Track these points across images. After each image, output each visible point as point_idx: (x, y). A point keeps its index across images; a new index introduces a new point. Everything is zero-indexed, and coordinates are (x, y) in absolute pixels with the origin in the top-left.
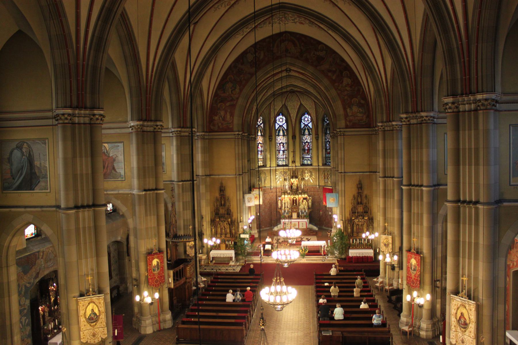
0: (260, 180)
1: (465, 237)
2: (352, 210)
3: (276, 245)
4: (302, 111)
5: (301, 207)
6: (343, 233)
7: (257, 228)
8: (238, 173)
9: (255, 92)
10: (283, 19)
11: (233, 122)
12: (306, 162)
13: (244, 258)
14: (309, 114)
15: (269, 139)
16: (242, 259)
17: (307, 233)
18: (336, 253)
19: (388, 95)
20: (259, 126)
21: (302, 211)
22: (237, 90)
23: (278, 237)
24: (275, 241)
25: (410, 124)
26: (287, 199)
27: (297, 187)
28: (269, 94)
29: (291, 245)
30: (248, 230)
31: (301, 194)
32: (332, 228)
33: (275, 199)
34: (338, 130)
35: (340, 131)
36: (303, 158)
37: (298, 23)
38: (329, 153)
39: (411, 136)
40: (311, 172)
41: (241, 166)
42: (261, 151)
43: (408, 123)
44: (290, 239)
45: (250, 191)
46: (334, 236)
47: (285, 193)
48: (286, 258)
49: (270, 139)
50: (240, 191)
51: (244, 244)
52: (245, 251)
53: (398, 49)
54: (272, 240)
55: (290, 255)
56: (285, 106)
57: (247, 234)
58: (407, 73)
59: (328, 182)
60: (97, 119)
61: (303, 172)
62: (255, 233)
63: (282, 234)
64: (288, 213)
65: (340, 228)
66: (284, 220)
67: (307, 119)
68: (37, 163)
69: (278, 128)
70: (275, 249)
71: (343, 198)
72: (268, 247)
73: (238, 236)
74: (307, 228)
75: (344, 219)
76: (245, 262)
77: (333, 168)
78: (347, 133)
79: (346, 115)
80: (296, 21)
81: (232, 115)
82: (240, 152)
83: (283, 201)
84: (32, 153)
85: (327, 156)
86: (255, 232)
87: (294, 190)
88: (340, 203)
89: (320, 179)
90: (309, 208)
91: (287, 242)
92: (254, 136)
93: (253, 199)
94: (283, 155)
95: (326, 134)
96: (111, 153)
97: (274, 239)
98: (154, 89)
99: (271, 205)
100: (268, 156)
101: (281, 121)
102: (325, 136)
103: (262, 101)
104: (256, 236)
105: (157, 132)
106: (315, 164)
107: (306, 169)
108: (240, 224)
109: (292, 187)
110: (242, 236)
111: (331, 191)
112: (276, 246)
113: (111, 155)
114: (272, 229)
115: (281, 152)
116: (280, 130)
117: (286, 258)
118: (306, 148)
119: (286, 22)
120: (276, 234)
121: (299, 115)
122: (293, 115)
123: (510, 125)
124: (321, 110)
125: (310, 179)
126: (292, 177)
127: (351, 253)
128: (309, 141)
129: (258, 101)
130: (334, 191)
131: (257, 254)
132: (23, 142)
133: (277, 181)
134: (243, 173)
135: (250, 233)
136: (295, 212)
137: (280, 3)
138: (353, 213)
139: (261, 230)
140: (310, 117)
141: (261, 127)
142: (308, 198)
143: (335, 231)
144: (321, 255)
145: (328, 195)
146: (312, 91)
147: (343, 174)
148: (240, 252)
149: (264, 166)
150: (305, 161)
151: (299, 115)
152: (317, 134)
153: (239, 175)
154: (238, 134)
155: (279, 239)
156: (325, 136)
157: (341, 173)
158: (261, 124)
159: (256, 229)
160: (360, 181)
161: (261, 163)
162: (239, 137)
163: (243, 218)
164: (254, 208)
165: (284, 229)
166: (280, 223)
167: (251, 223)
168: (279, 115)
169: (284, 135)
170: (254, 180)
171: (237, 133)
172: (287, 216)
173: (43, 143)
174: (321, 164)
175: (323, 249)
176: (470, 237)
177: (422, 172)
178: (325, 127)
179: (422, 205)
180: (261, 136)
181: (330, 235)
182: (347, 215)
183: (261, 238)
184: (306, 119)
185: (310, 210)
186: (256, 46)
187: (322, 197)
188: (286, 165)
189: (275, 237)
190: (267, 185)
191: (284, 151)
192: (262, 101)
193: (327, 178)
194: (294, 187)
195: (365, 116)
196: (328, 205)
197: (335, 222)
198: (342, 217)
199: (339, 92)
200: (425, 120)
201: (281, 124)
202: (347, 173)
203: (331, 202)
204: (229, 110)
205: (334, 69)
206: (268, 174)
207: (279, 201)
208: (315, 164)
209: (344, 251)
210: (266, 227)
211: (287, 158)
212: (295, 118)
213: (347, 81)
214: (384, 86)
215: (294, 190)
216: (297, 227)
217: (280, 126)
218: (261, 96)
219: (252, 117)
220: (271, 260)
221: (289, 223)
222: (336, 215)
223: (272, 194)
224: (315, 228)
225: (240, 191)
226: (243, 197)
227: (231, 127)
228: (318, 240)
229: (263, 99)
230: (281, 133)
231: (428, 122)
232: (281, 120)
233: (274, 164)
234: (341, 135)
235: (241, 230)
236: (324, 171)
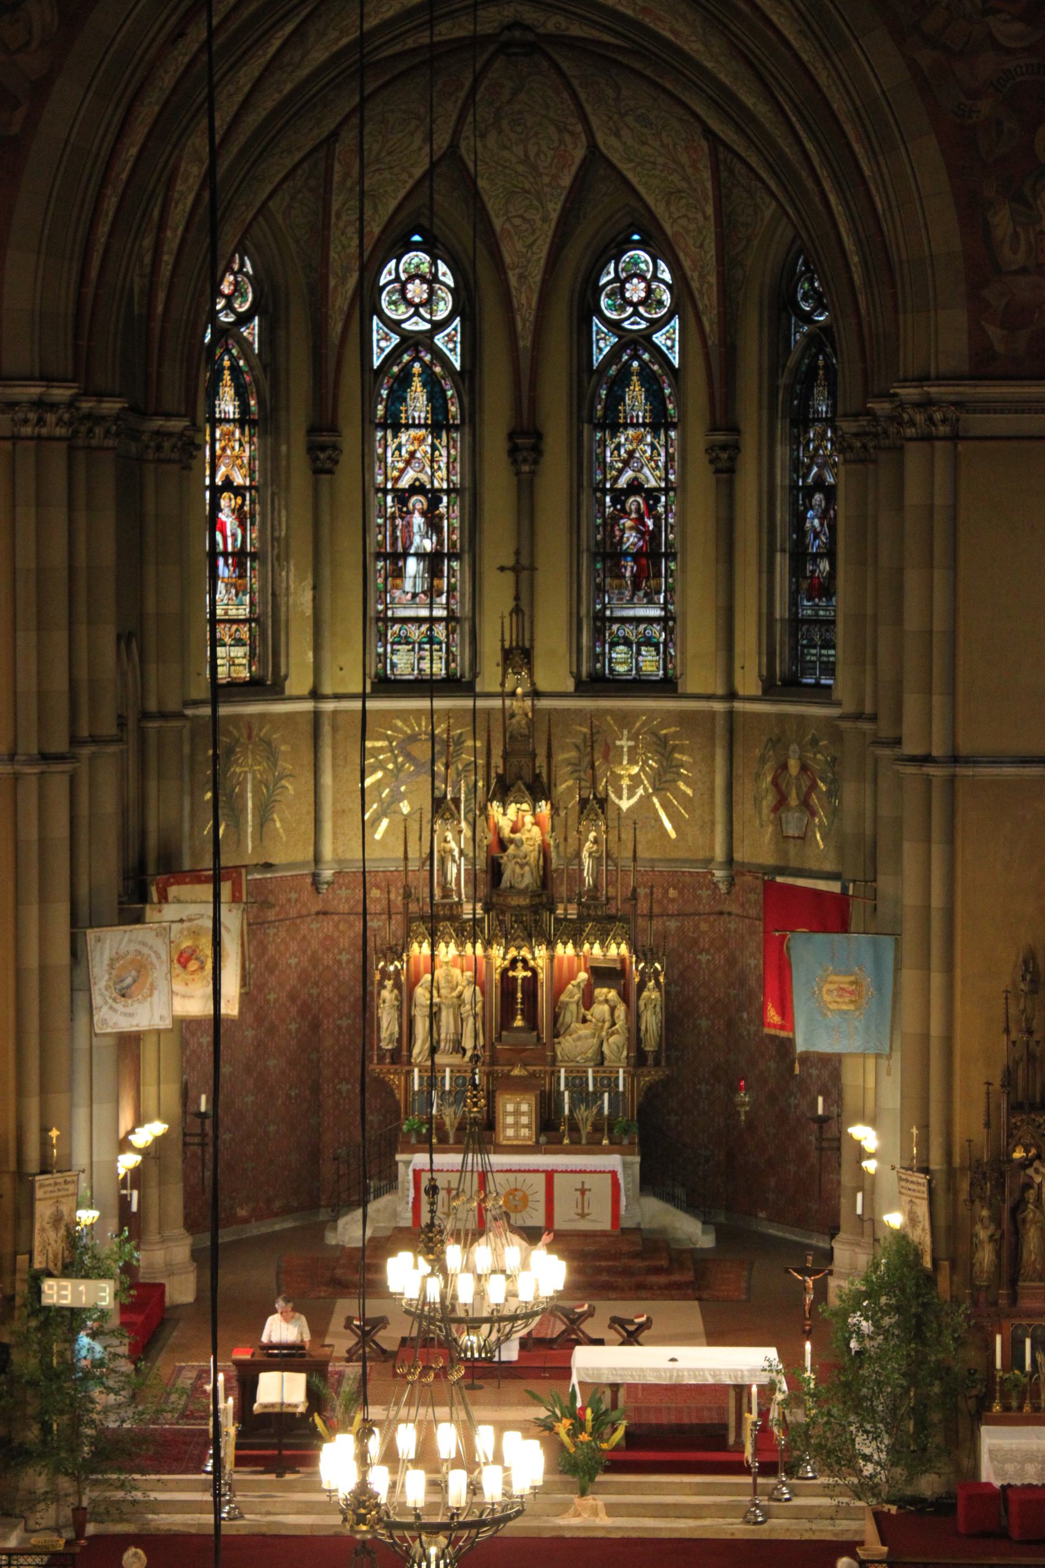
0: (223, 804)
2: (1009, 1078)
3: (353, 1370)
4: (603, 221)
5: (576, 1043)
6: (930, 1279)
7: (191, 1225)
8: (30, 746)
9: (198, 34)
12: (619, 661)
13: (65, 1483)
14: (660, 246)
15: (313, 449)
16: (54, 1496)
17: (619, 1274)
18: (871, 1448)
20: (222, 333)
21: (577, 1084)
23: (374, 1308)
24: (340, 1342)
26: (451, 968)
27: (546, 877)
28: (319, 56)
29: (485, 1372)
30: (107, 1244)
31: (575, 934)
32: (833, 1231)
33: (349, 973)
34: (909, 393)
35: (925, 404)
36: (601, 622)
38: (825, 589)
40: (663, 748)
41: (60, 683)
42: (240, 557)
44: (473, 1324)
45: (134, 899)
46: (855, 1302)
47: (437, 920)
48: (438, 1486)
49: (323, 457)
50: (44, 899)
51: (71, 1367)
52: (76, 1423)
54: (318, 1330)
55: (467, 1461)
56: (451, 168)
57: (102, 1274)
59: (803, 838)
61: (596, 749)
62: (170, 1270)
63: (405, 1275)
64: (457, 1096)
65: (900, 1237)
66: (420, 1160)
67: (639, 287)
70: (338, 1404)
71: (937, 979)
72: (280, 1390)
73: (22, 1289)
74: (621, 1232)
75: (936, 1163)
76: (79, 1528)
77: (858, 717)
78: (978, 423)
82: (58, 557)
83: (421, 993)
85: (806, 610)
86: (172, 1262)
87: (518, 903)
88: (910, 1021)
89: (744, 809)
90: (639, 1058)
91: (449, 1345)
92: (177, 425)
93: (159, 974)
94: (432, 592)
95: (801, 420)
97: (337, 1323)
99: (315, 1026)
100: (301, 599)
101: (416, 297)
102: (796, 441)
103: (253, 120)
104: (182, 1290)
106: (700, 677)
107: (625, 719)
108: (44, 1187)
109: (495, 870)
110: (58, 1292)
111: (831, 915)
112: (348, 1387)
114: (318, 1232)
115: (412, 566)
116: (404, 380)
117: (438, 1486)
118: (631, 539)
120: (362, 1271)
121: (574, 255)
122: (526, 252)
124: (769, 210)
125: (654, 806)
126: (503, 790)
127: (999, 1457)
128: (651, 480)
129: (221, 121)
130: (857, 913)
131: (180, 1450)
133: (371, 815)
134: (75, 741)
135: (128, 1269)
136: (520, 1086)
138: (1015, 1108)
139: (225, 1236)
141: (244, 345)
142: (636, 968)
143: (863, 1260)
144: (740, 1468)
145: (809, 953)
146: (694, 47)
147: (935, 771)
148: (33, 1433)
149: (264, 685)
150: (620, 653)
151: (574, 255)
152: (724, 422)
153: (45, 757)
154: (41, 405)
155: (381, 1322)
156: (796, 441)
157: (926, 759)
158: (243, 319)
159: (177, 1229)
161: (233, 661)
162: (53, 426)
163: (67, 1137)
164: (170, 1048)
165: (427, 1239)
166: (390, 1181)
167: (137, 1177)
169: (438, 425)
170: (178, 810)
171: (34, 391)
172: (450, 1117)
174: (748, 682)
175: (752, 1417)
178: (793, 365)
180: (243, 420)
181: (821, 1291)
182: (970, 1124)
183: (227, 1312)
184: (636, 290)
185: (650, 1076)
187: (753, 961)
188: (453, 685)
189: (346, 1307)
190: (288, 849)
191: (433, 561)
192: (253, 120)
193: (805, 804)
194: (520, 875)
196: (810, 1036)
197: (865, 1183)
198: (924, 1142)
202: (971, 761)
203: (834, 1010)
206: (291, 755)
207: (388, 994)
208: (700, 677)
209: (936, 1440)
210: (259, 1215)
211: (464, 623)
215: (518, 903)
216: (536, 1218)
217: (410, 342)
218: (247, 75)
219: (168, 259)
220: (309, 1508)
221: (471, 1183)
222: (873, 1122)
223: (327, 926)
224: (691, 1231)
225: (44, 899)
226: (77, 954)
228: (716, 1337)
229: (268, 102)
230: (417, 403)
232: (416, 291)
233: (347, 674)
234: (927, 438)
235: (46, 1243)
236: (778, 743)
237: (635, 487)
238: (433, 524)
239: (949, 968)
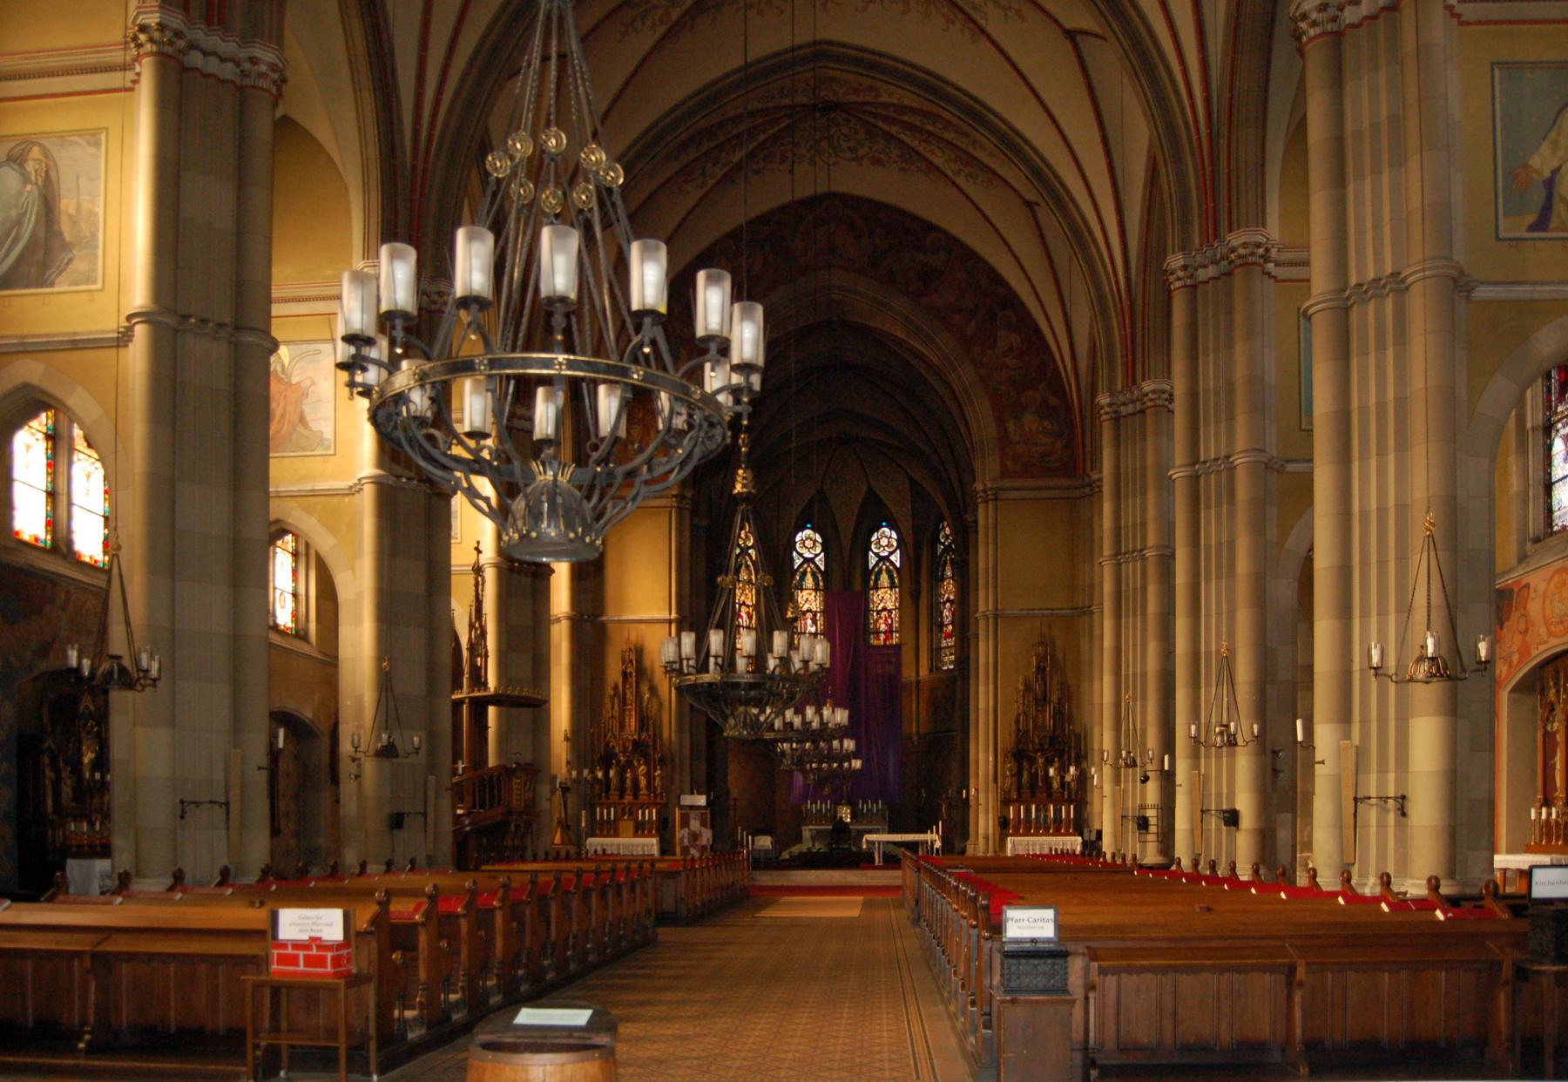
1: (1367, 393)
10: (824, 144)
19: (1131, 307)
25: (1194, 287)
37: (866, 162)
39: (1200, 316)
53: (1161, 67)
58: (1188, 129)
67: (885, 542)
68: (67, 205)
78: (1002, 495)
79: (1004, 441)
80: (862, 152)
84: (53, 175)
96: (296, 372)
101: (808, 545)
113: (294, 381)
119: (833, 159)
123: (1493, 64)
128: (890, 606)
132: (28, 142)
137: (815, 43)
140: (894, 535)
160: (1045, 642)
168: (803, 528)
173: (89, 144)
176: (1381, 386)
177: (1231, 418)
179: (1232, 515)
184: (884, 542)
195: (1059, 444)
200: (1240, 257)
213: (1007, 339)
214: (1117, 282)
217: (807, 560)
231: (1250, 259)
232: (809, 543)
237: (884, 609)
238: (814, 622)
239: (996, 638)
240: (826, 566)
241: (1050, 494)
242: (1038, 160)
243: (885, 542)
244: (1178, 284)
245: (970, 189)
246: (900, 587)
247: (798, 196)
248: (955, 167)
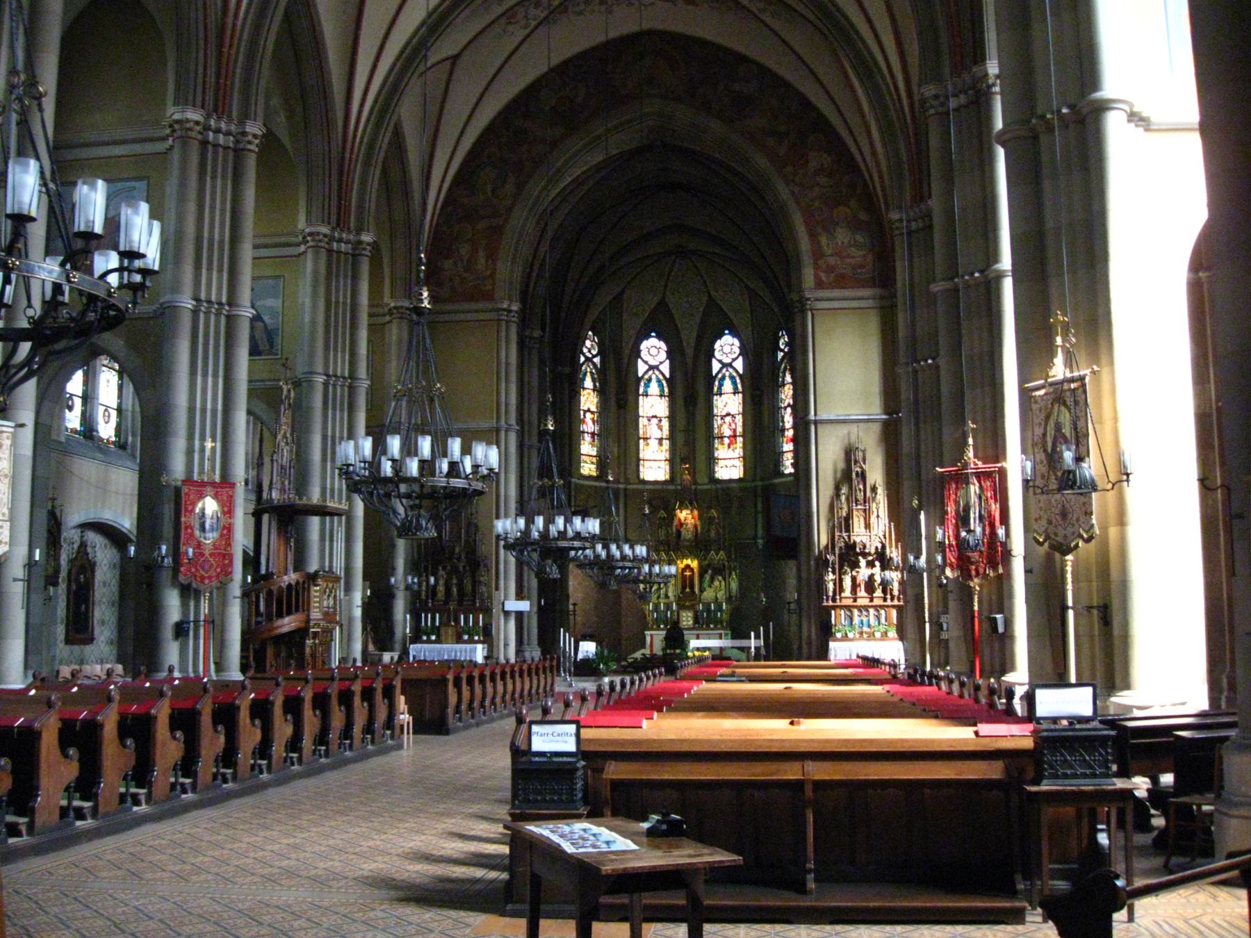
11: (492, 275)
14: (734, 333)
22: (510, 188)
43: (940, 109)
60: (249, 142)
67: (727, 348)
69: (646, 372)
81: (492, 255)
90: (729, 599)
98: (245, 36)
101: (653, 352)
105: (243, 150)
168: (648, 337)
186: (563, 71)
199: (796, 190)
201: (653, 362)
204: (484, 242)
205: (783, 129)
212: (692, 342)
217: (652, 368)
227: (489, 287)
238: (660, 428)
240: (671, 373)
241: (855, 304)
242: (399, 64)
243: (727, 348)
244: (932, 111)
245: (776, 25)
246: (743, 393)
247: (612, 35)
248: (761, 5)
